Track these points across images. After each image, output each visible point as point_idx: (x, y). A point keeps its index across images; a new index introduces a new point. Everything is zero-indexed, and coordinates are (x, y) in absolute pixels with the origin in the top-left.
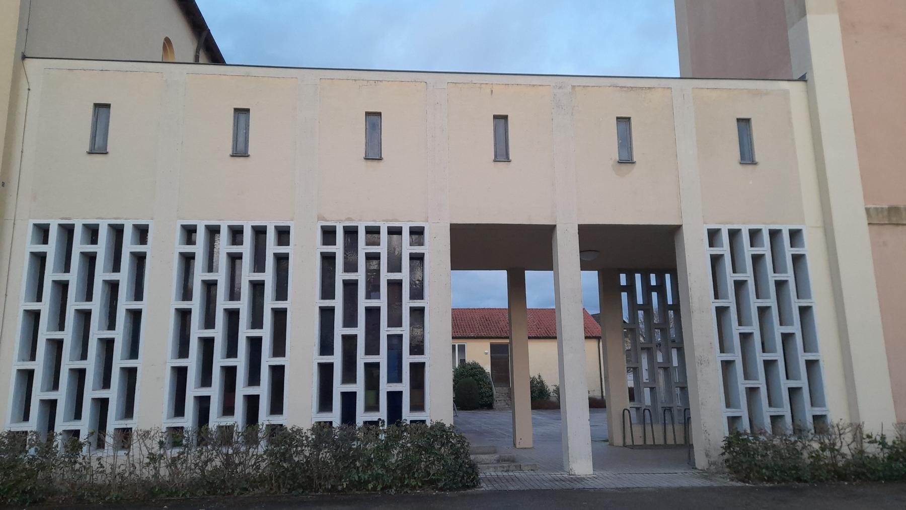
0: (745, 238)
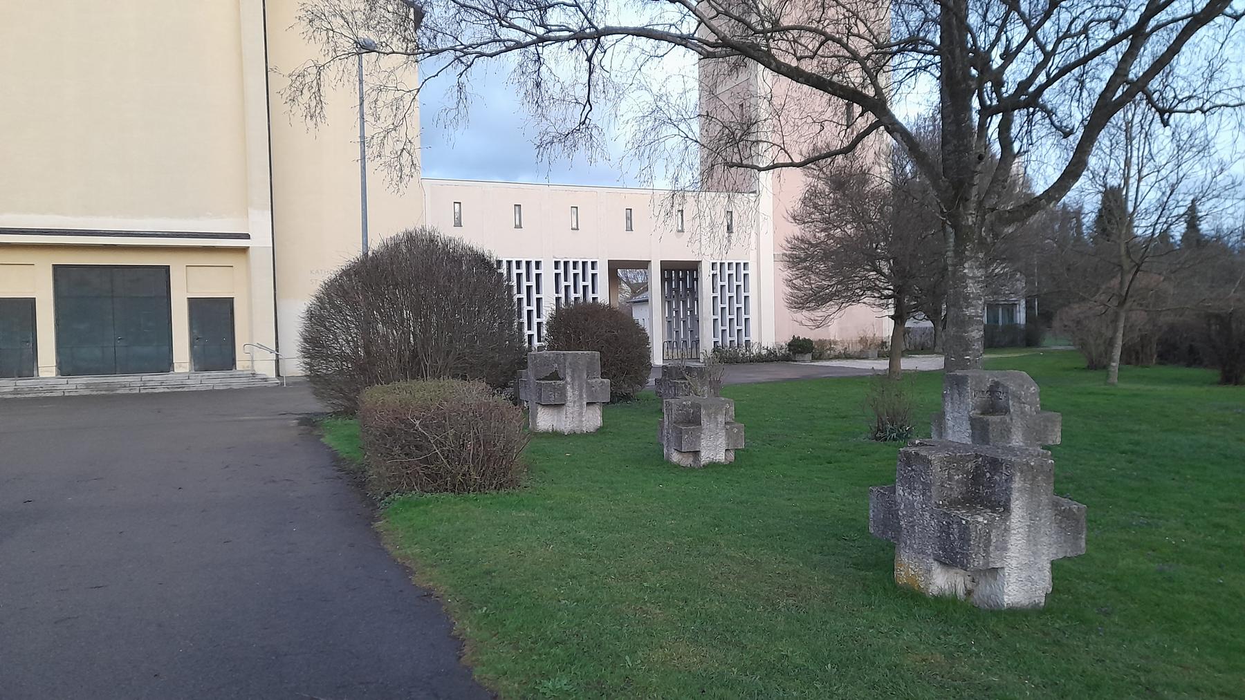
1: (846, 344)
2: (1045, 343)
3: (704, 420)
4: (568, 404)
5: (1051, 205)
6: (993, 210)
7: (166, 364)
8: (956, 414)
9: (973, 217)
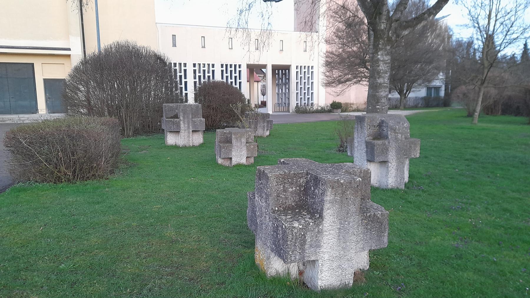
0: (311, 68)
2: (453, 105)
3: (234, 141)
4: (181, 131)
5: (431, 18)
6: (397, 21)
7: (34, 110)
8: (359, 140)
9: (384, 25)
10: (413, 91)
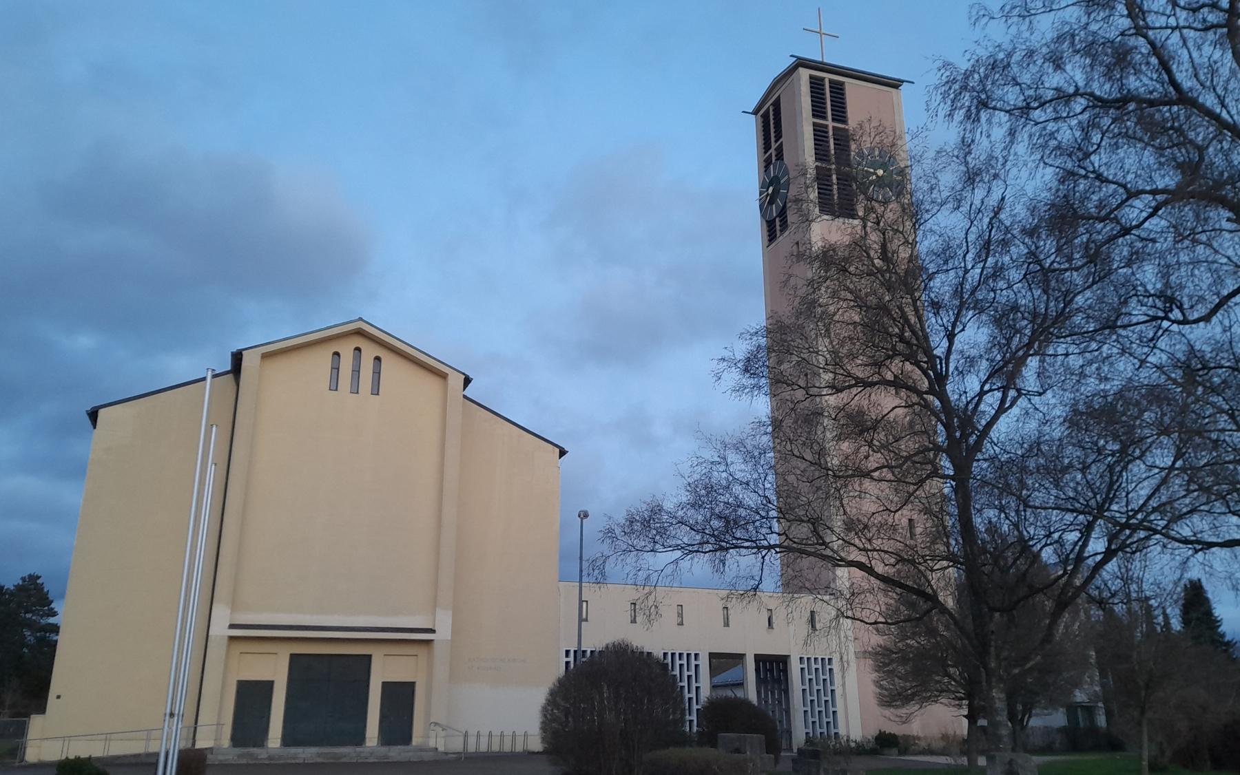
0: (693, 657)
1: (929, 740)
10: (1037, 715)
